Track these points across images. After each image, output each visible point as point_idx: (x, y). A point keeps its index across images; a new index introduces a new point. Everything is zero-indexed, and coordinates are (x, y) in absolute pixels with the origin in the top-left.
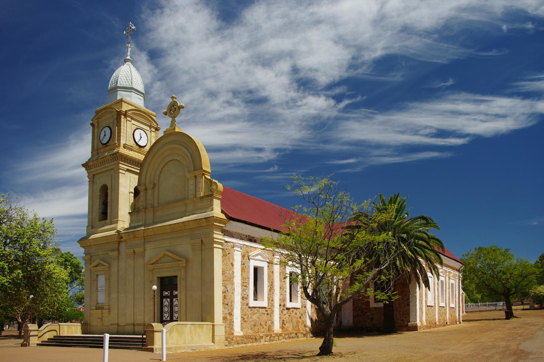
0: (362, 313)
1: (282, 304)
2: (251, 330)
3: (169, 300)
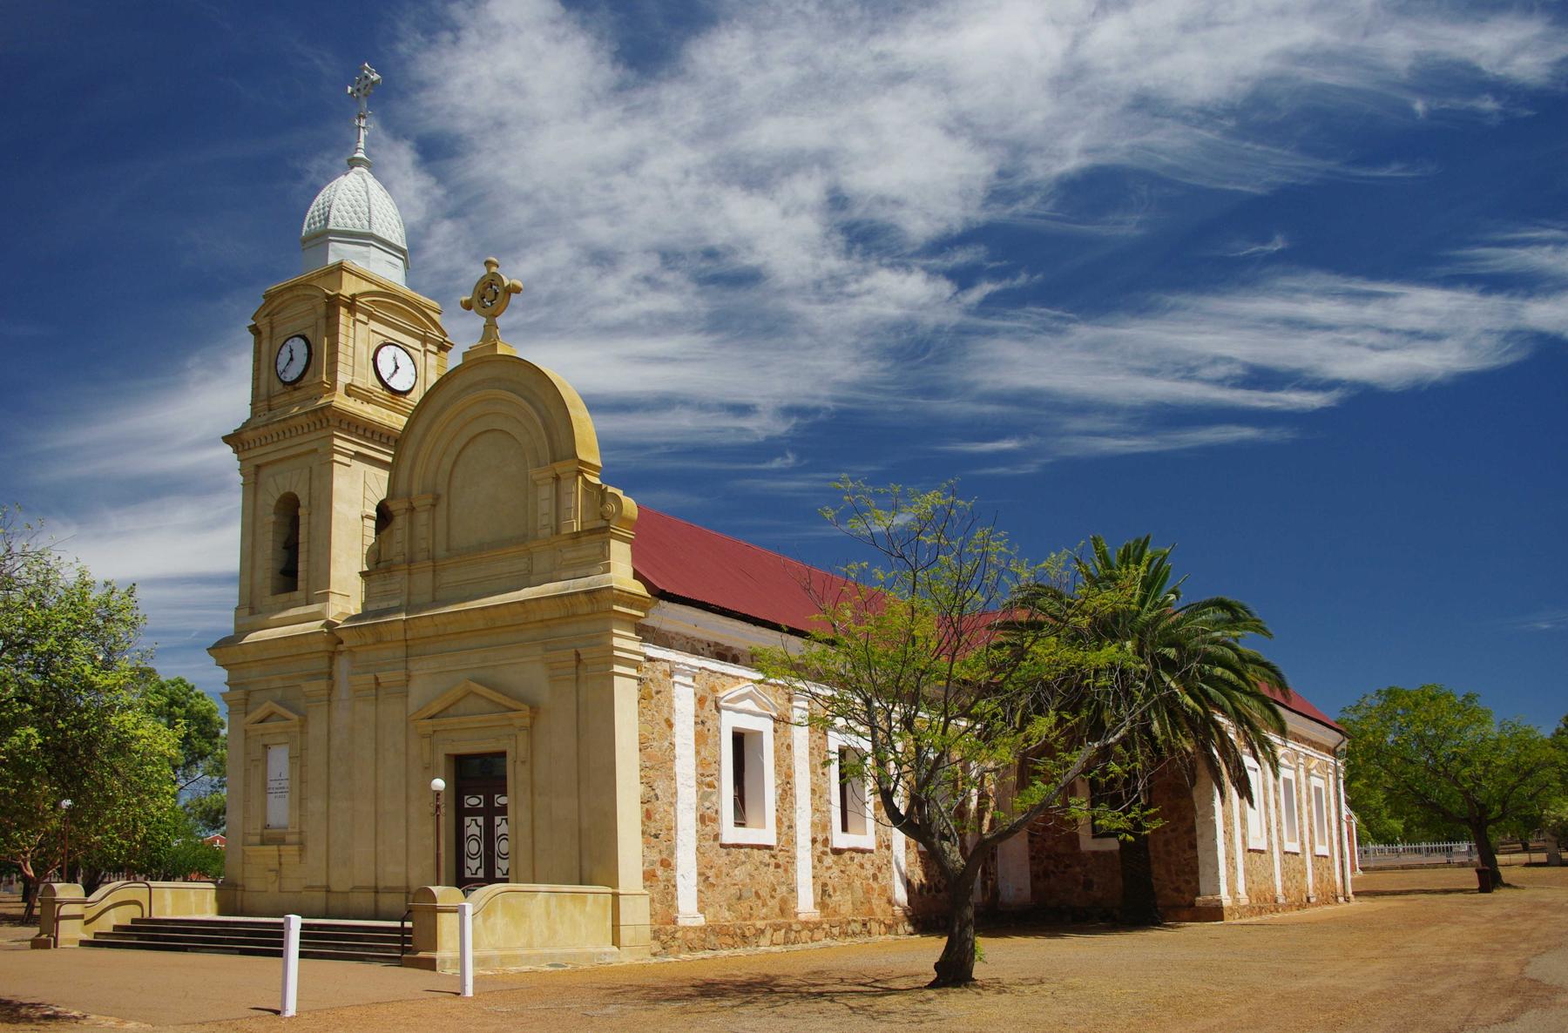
0: (1057, 867)
1: (820, 838)
3: (480, 820)
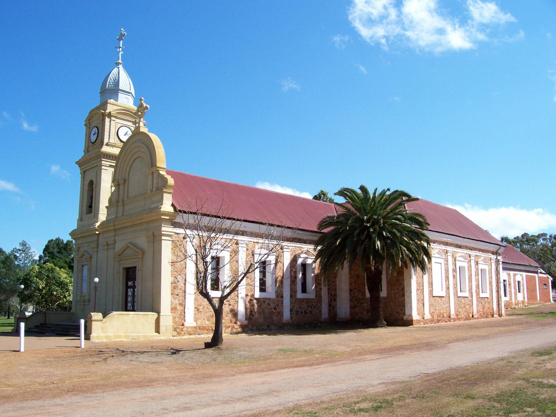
0: (358, 304)
1: (250, 294)
2: (208, 321)
3: (132, 290)
